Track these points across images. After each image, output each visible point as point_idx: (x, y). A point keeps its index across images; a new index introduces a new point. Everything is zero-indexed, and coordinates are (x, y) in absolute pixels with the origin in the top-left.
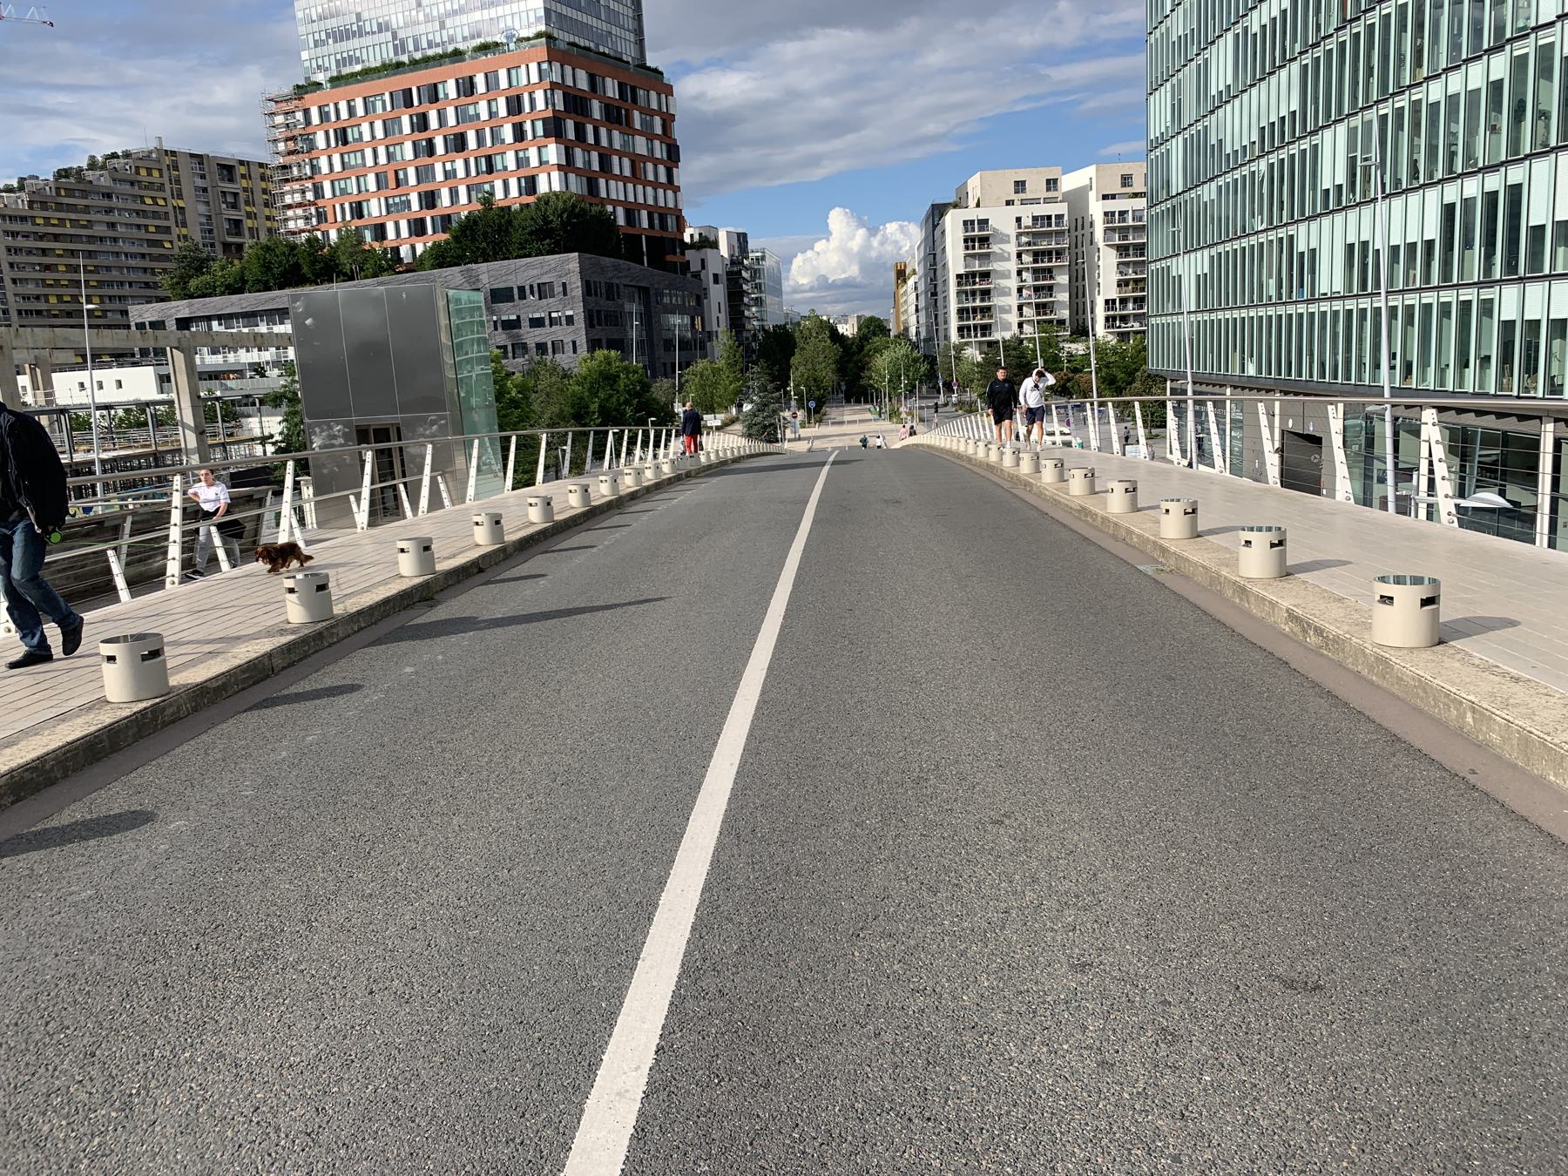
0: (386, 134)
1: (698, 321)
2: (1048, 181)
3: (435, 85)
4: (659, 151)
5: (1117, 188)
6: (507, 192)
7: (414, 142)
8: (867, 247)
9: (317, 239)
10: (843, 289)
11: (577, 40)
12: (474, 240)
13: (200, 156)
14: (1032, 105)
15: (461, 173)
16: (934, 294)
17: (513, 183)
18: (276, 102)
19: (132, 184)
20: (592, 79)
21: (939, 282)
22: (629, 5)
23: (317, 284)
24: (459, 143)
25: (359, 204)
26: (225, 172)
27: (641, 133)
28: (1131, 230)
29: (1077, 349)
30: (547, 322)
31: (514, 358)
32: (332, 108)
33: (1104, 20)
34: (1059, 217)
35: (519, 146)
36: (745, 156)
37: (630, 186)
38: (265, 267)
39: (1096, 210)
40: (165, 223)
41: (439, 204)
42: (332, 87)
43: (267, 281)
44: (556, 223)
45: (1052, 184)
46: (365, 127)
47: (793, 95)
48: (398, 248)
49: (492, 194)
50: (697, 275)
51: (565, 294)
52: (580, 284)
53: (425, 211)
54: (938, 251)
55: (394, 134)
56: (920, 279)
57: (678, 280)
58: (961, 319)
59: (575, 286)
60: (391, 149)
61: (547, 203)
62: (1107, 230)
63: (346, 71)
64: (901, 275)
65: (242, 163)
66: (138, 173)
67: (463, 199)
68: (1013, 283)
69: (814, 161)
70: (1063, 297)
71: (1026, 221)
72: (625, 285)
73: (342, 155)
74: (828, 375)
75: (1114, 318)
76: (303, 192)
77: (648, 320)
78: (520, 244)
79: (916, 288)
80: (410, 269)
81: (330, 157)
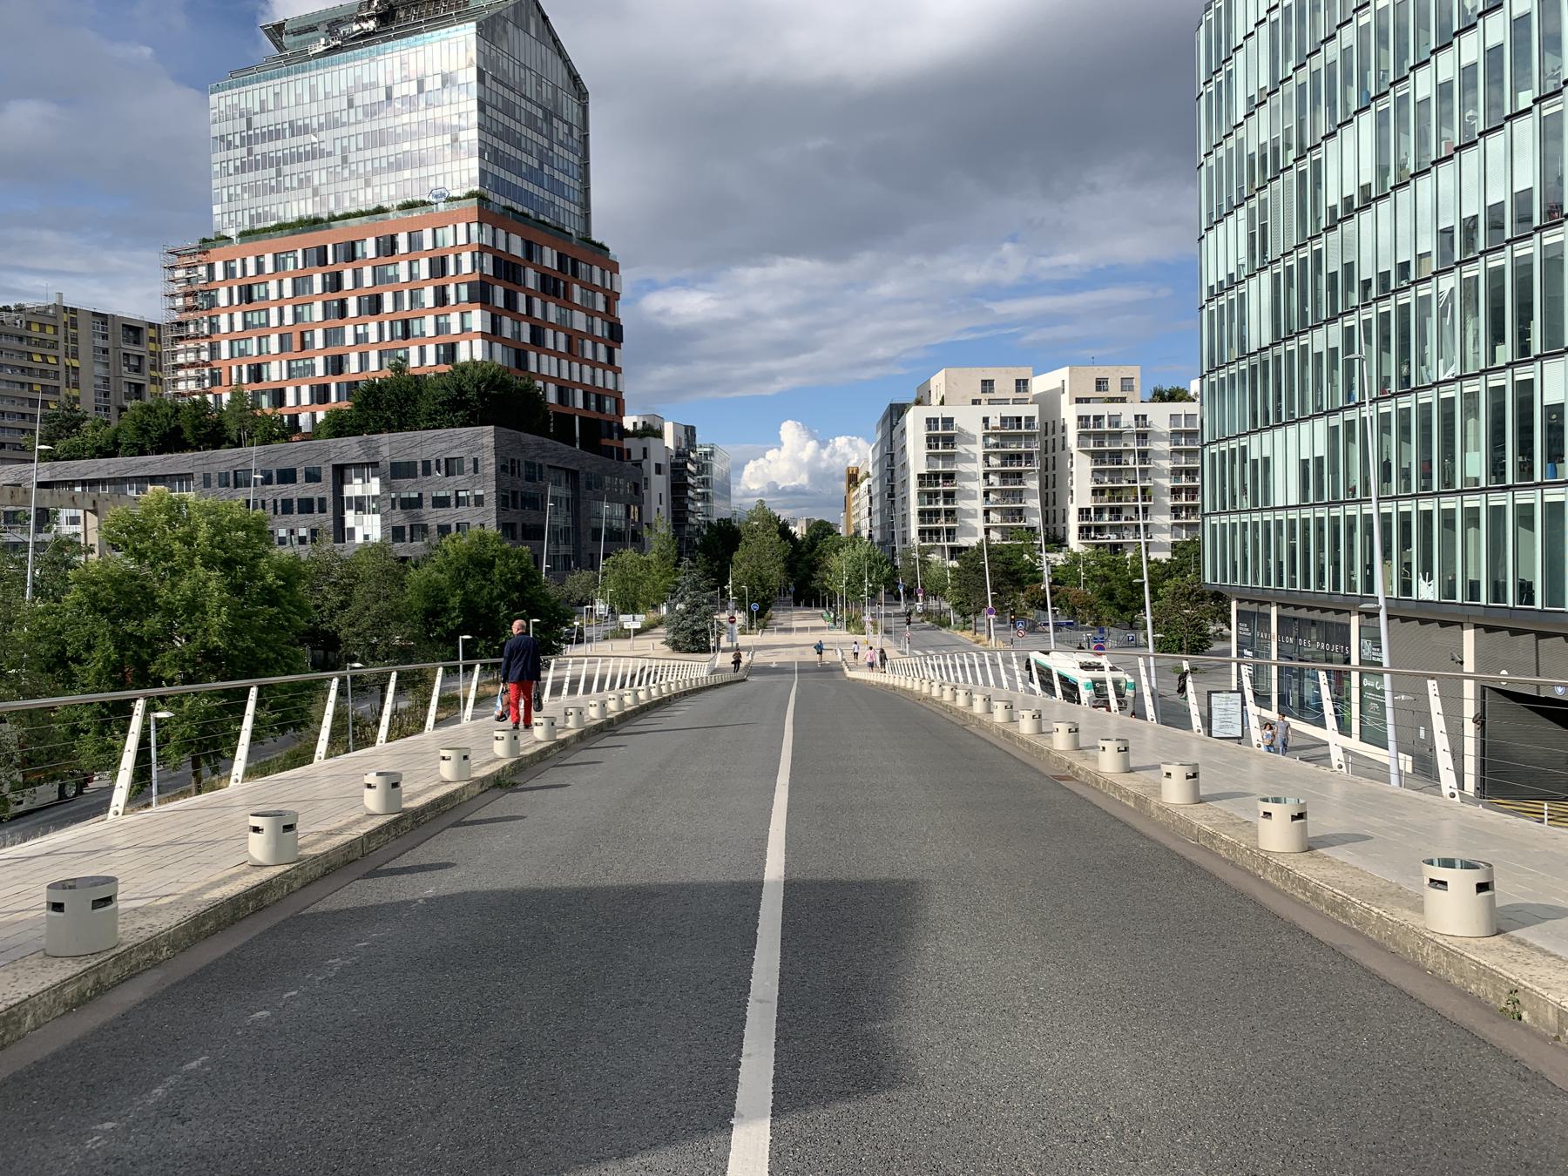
0: (295, 293)
1: (634, 509)
2: (1018, 382)
3: (353, 244)
4: (600, 328)
5: (1091, 392)
6: (422, 359)
7: (325, 303)
8: (817, 458)
9: (206, 403)
10: (794, 495)
11: (514, 205)
12: (377, 408)
13: (105, 316)
14: (973, 336)
15: (373, 338)
16: (892, 495)
17: (431, 351)
18: (179, 255)
19: (21, 339)
20: (528, 246)
21: (897, 483)
22: (575, 177)
23: (200, 450)
24: (373, 305)
25: (259, 366)
26: (131, 334)
27: (580, 308)
28: (1107, 437)
29: (1055, 559)
30: (453, 502)
31: (412, 541)
32: (239, 264)
33: (1044, 262)
34: (1030, 419)
35: (440, 310)
36: (703, 369)
37: (565, 363)
38: (140, 428)
39: (1069, 413)
40: (55, 383)
41: (346, 370)
42: (241, 242)
43: (143, 445)
44: (471, 393)
45: (1022, 384)
46: (273, 285)
47: (751, 316)
48: (296, 416)
49: (406, 360)
50: (638, 464)
51: (476, 471)
52: (493, 461)
53: (330, 376)
54: (897, 451)
55: (304, 293)
56: (874, 481)
57: (613, 466)
58: (922, 521)
59: (488, 462)
60: (299, 309)
61: (463, 372)
62: (1080, 435)
63: (258, 226)
64: (853, 479)
65: (152, 325)
66: (28, 327)
67: (373, 364)
68: (978, 487)
69: (769, 377)
70: (1034, 503)
71: (995, 422)
72: (549, 466)
73: (245, 314)
74: (776, 574)
75: (1089, 529)
76: (198, 351)
77: (575, 505)
78: (430, 414)
79: (869, 491)
80: (307, 437)
81: (231, 315)
